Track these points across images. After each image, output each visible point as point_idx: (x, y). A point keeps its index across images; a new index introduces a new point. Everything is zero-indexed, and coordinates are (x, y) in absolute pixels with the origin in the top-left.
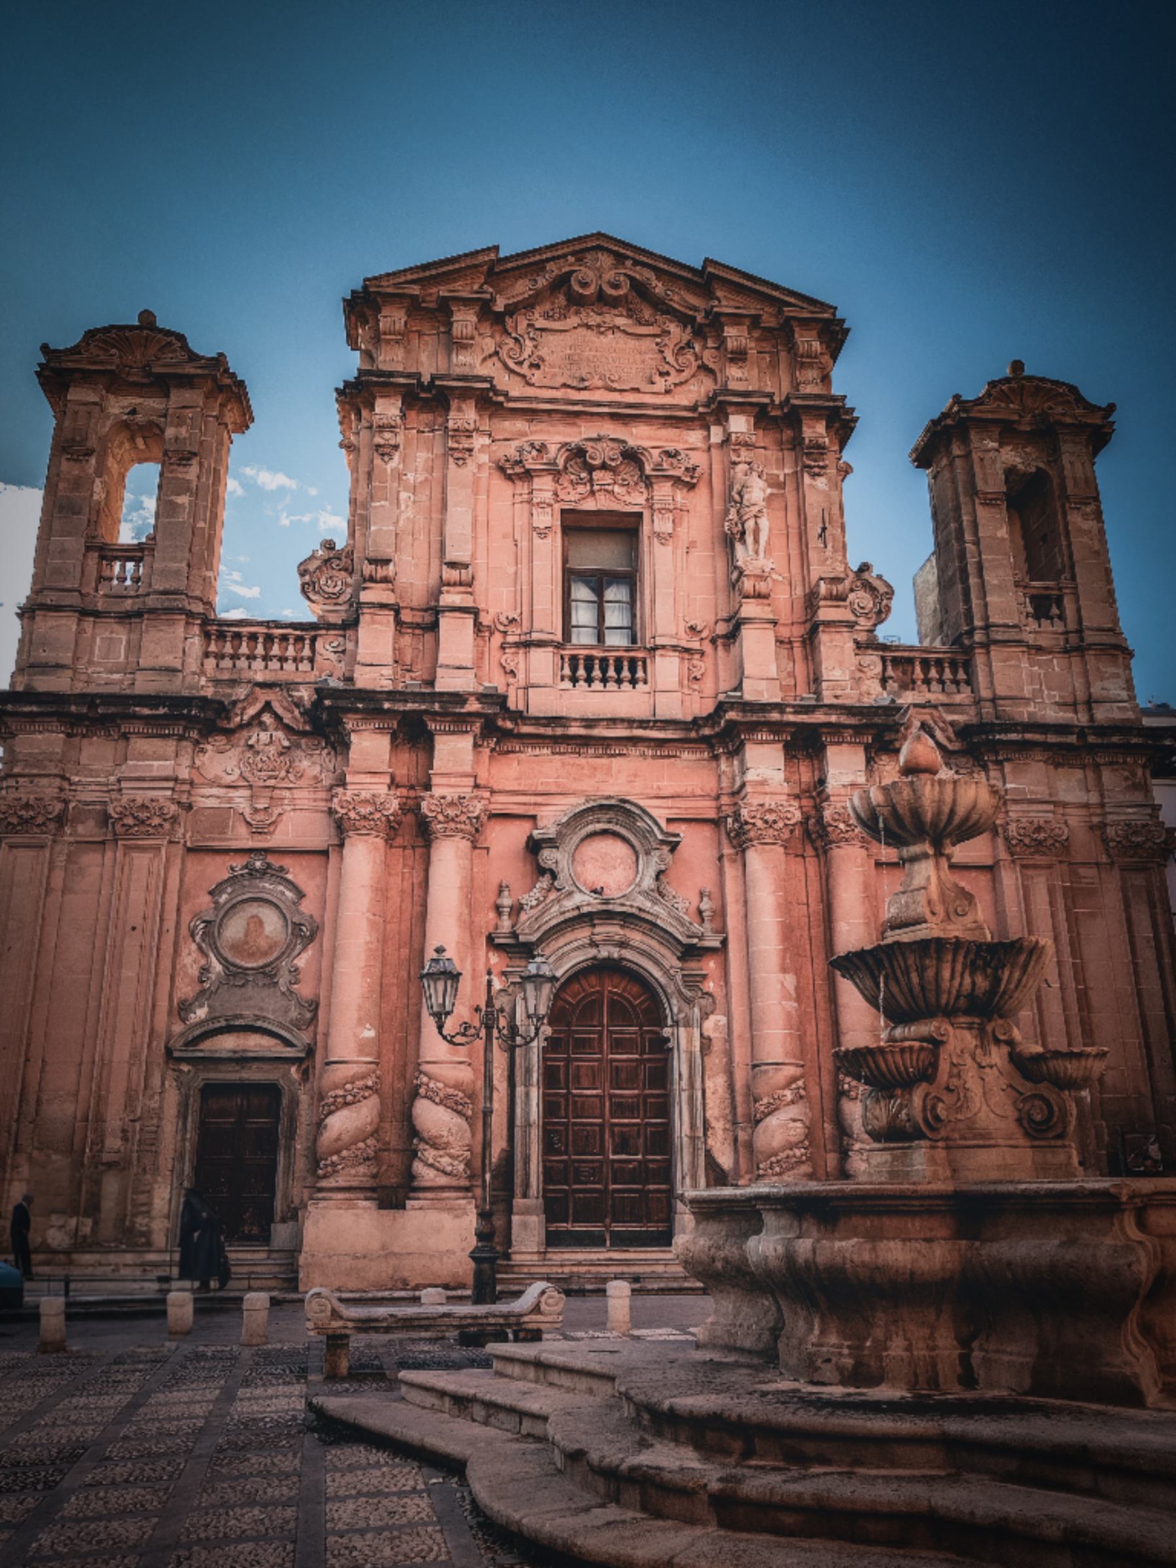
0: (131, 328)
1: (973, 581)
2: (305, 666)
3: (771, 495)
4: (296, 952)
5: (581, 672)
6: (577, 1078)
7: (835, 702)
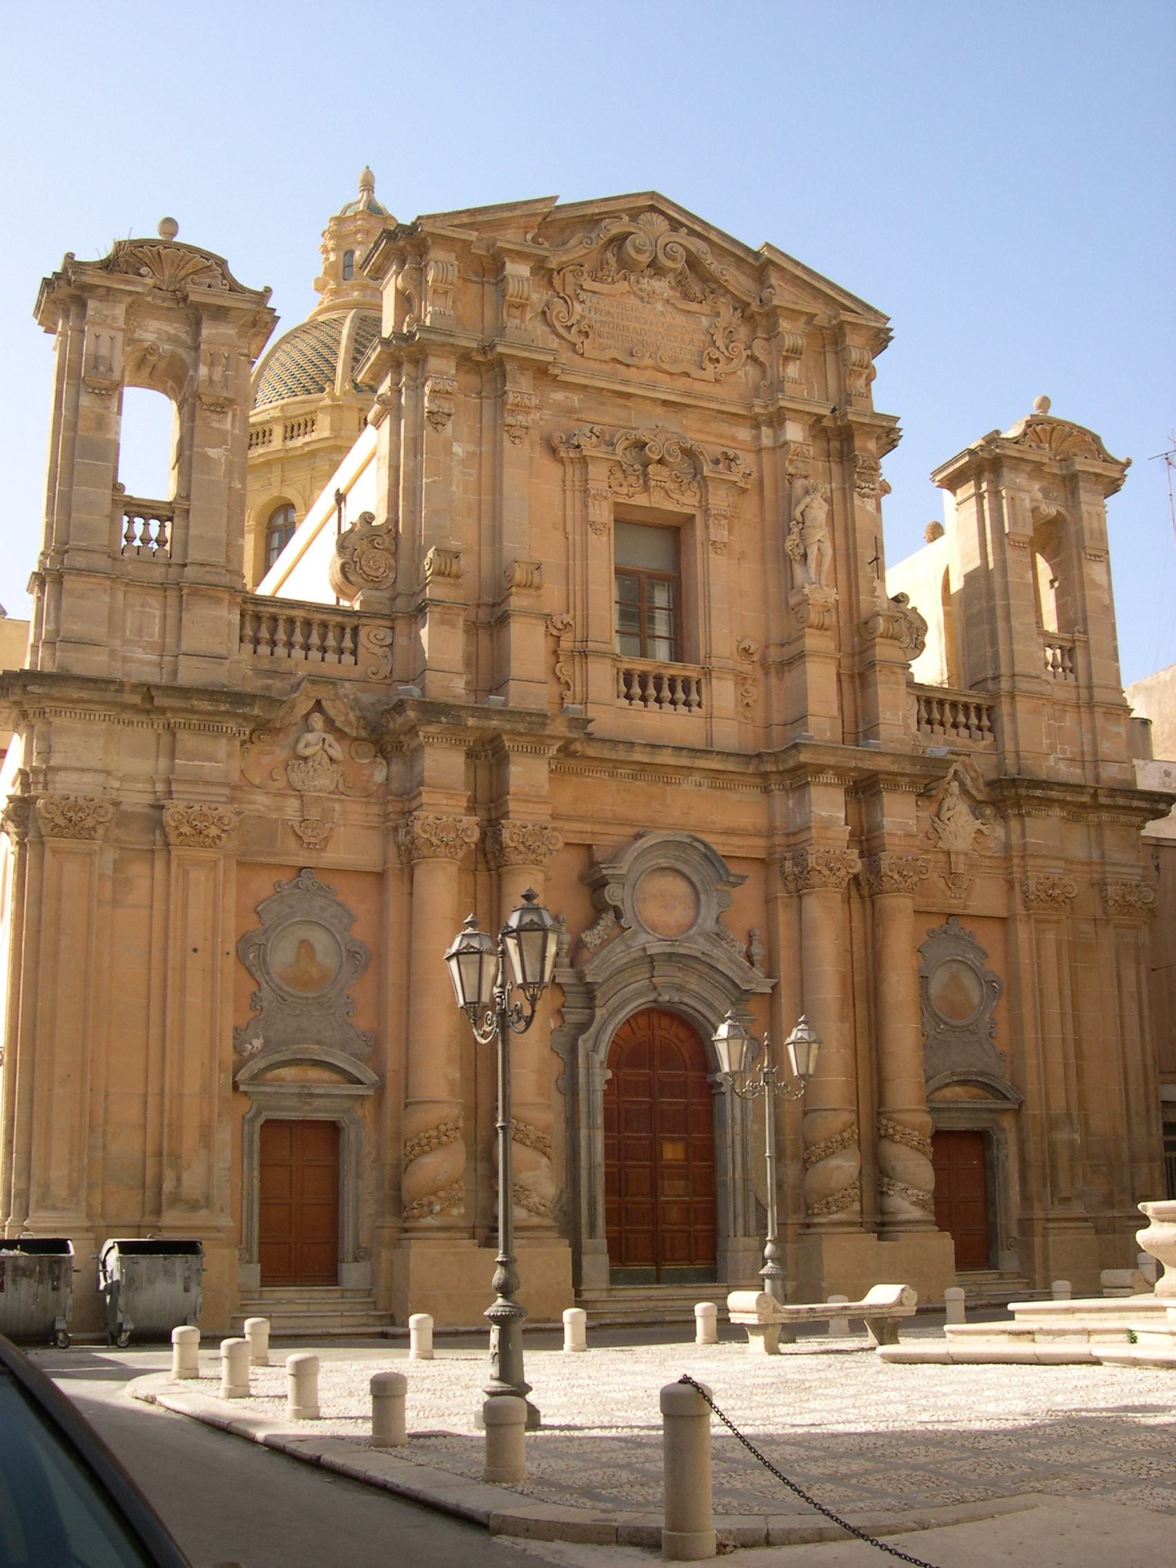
1: (1000, 625)
2: (348, 659)
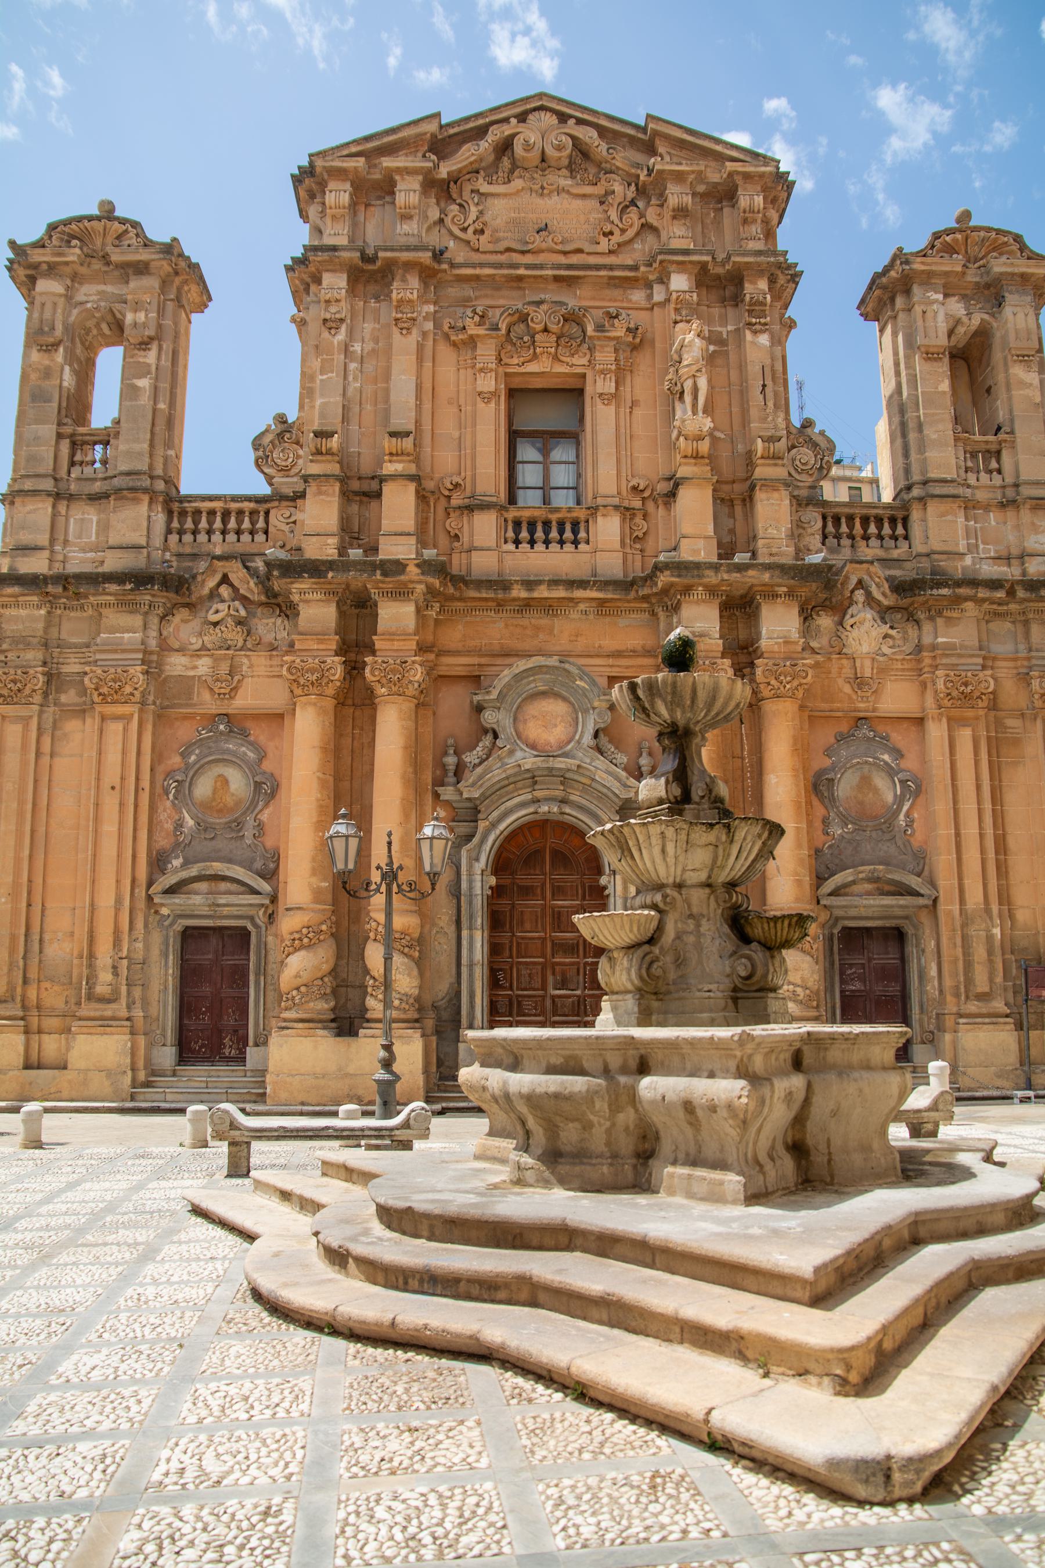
0: (90, 218)
3: (714, 352)
4: (259, 807)
5: (524, 534)
6: (522, 922)
7: (772, 560)
